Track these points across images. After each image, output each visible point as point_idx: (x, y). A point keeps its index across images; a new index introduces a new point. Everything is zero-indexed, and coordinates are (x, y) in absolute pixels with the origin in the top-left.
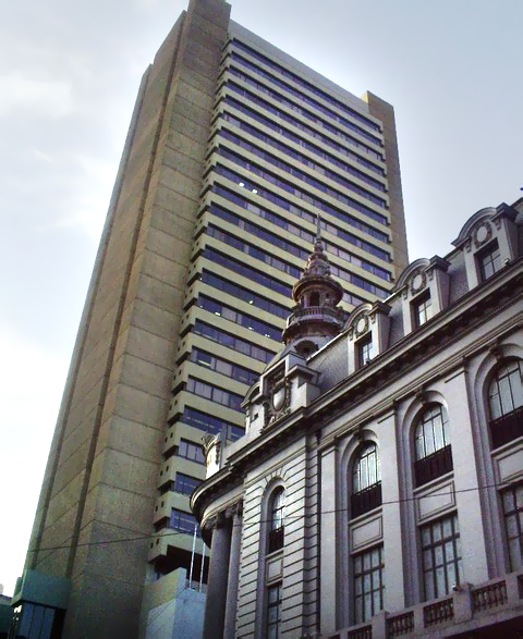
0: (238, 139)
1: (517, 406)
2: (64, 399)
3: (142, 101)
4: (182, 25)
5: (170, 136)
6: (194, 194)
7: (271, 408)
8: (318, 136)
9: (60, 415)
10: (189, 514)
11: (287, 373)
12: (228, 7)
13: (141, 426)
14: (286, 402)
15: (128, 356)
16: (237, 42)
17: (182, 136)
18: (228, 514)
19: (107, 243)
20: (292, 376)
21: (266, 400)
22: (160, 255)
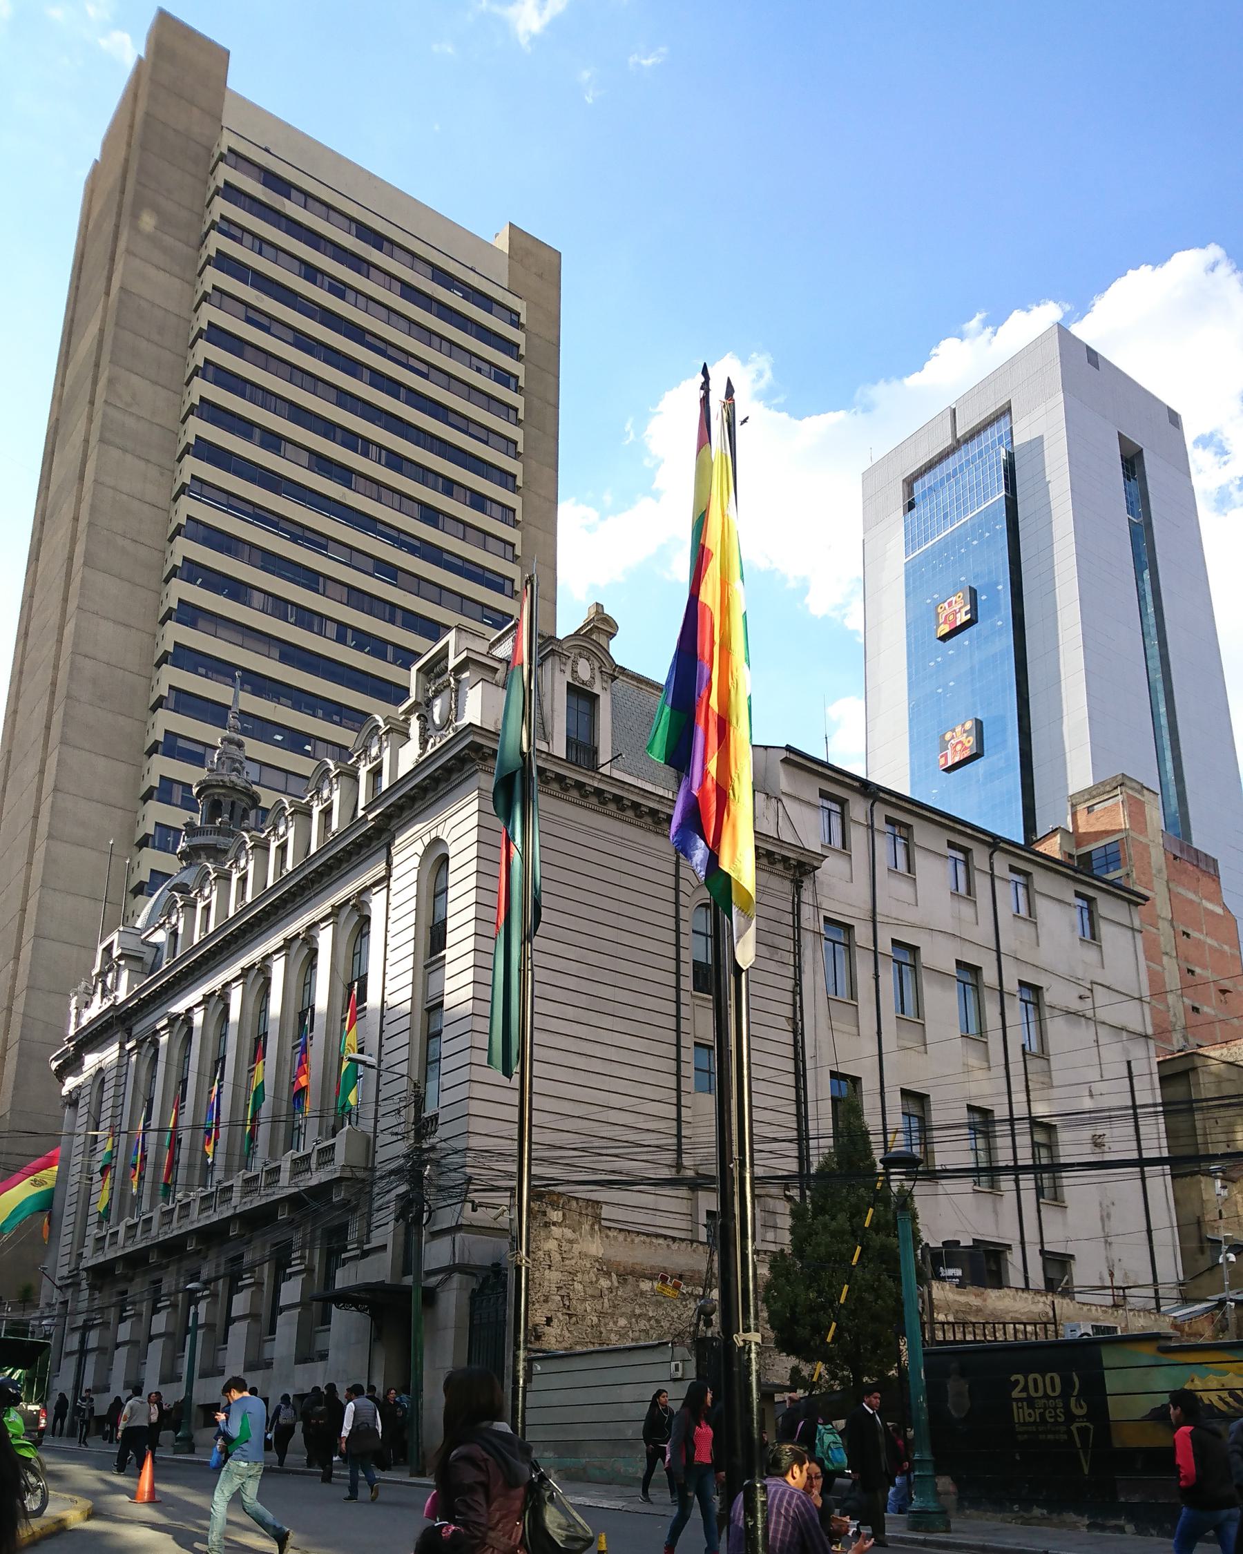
0: (236, 345)
1: (543, 909)
2: (75, 261)
3: (72, 320)
4: (135, 97)
5: (111, 381)
6: (165, 501)
7: (429, 725)
8: (420, 265)
9: (84, 200)
10: (561, 759)
11: (452, 663)
12: (221, 56)
13: (87, 901)
14: (456, 709)
15: (59, 795)
16: (236, 158)
17: (135, 379)
18: (74, 1096)
19: (79, 278)
20: (459, 669)
21: (423, 708)
22: (105, 618)
